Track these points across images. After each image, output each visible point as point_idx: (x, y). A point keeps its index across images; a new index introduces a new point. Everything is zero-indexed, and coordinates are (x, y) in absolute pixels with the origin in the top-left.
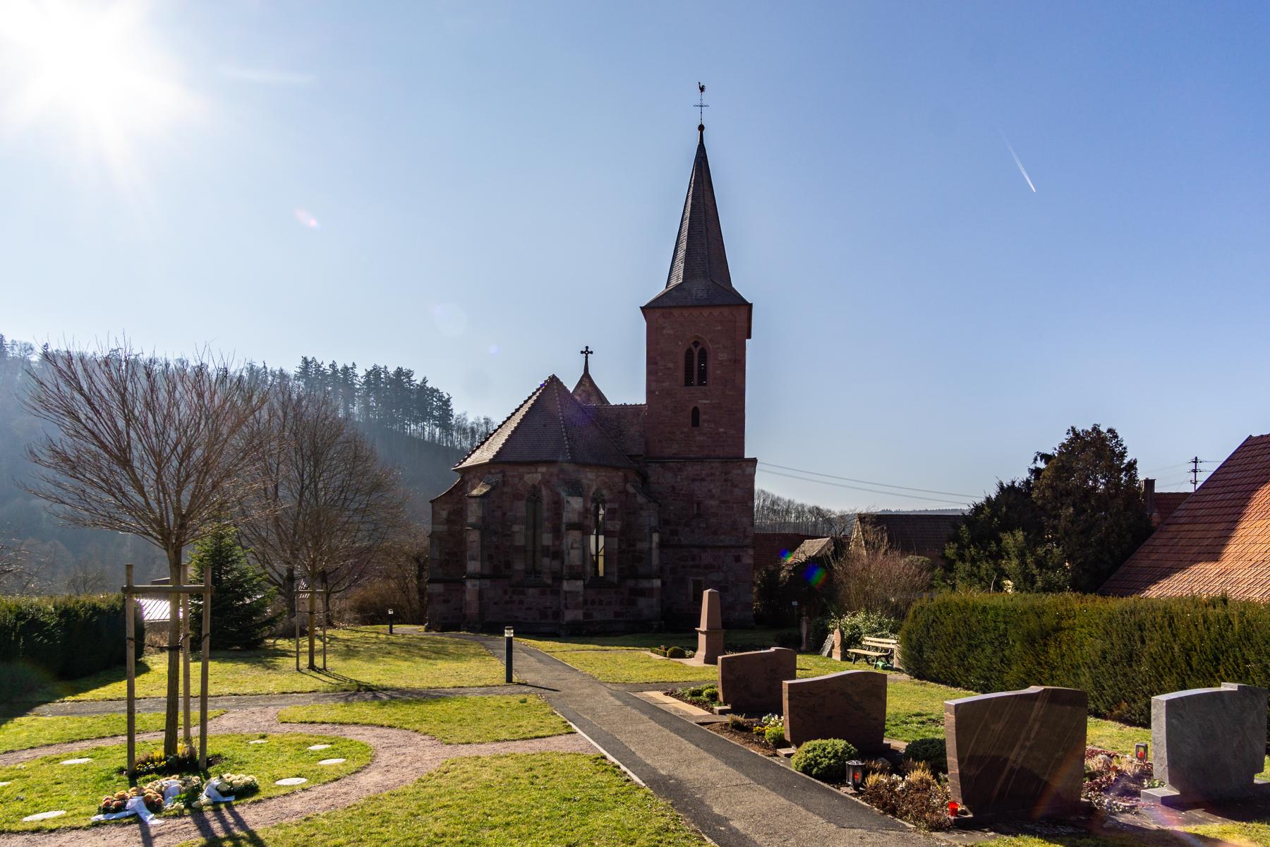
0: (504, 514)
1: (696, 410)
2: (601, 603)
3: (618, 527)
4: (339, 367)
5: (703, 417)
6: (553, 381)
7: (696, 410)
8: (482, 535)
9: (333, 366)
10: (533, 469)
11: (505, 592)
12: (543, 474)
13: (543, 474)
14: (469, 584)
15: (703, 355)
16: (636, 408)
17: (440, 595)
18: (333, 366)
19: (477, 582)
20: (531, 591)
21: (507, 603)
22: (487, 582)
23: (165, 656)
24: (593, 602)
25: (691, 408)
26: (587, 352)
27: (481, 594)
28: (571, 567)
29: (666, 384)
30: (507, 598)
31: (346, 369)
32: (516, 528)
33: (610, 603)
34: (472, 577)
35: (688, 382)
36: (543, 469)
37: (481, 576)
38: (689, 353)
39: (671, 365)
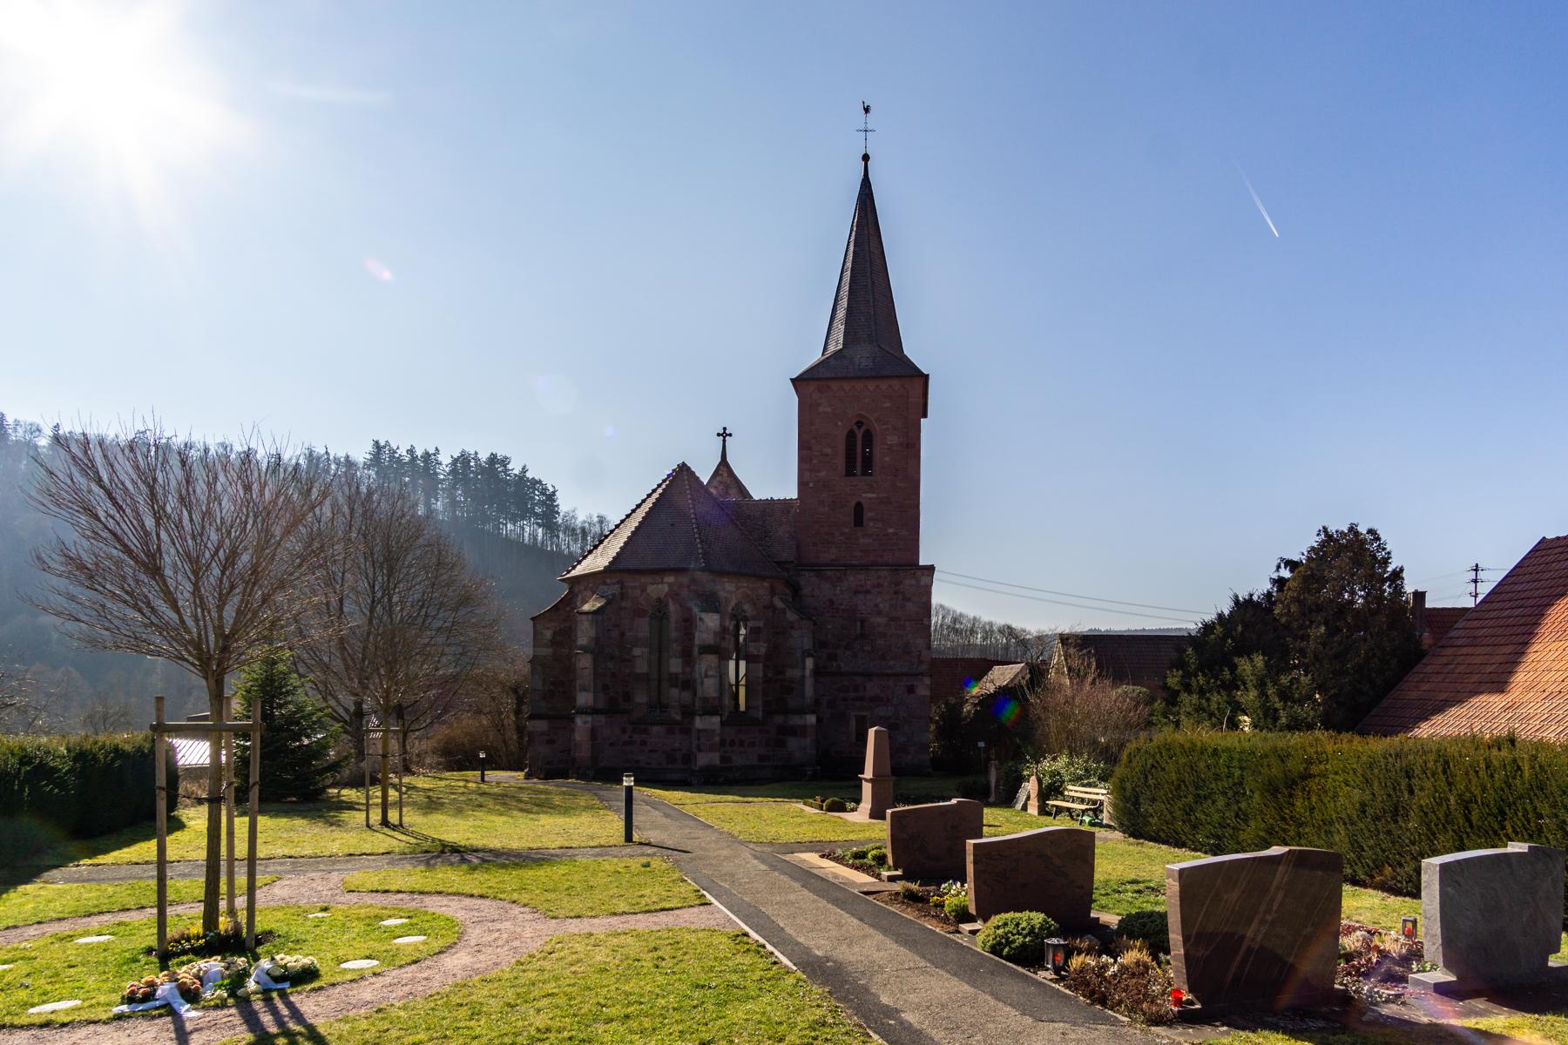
0: (623, 634)
1: (859, 506)
2: (742, 744)
3: (763, 650)
4: (419, 453)
5: (868, 515)
6: (683, 470)
7: (859, 506)
8: (595, 660)
9: (411, 451)
10: (658, 579)
11: (624, 731)
12: (670, 585)
13: (670, 585)
14: (579, 721)
15: (868, 438)
16: (786, 504)
17: (543, 734)
18: (411, 451)
19: (589, 718)
20: (655, 729)
21: (625, 743)
22: (602, 719)
24: (732, 743)
25: (853, 503)
26: (724, 434)
27: (593, 733)
28: (705, 700)
29: (823, 474)
30: (626, 737)
31: (427, 455)
32: (637, 651)
33: (753, 744)
34: (583, 711)
35: (849, 472)
36: (670, 579)
37: (594, 711)
38: (851, 436)
39: (828, 451)
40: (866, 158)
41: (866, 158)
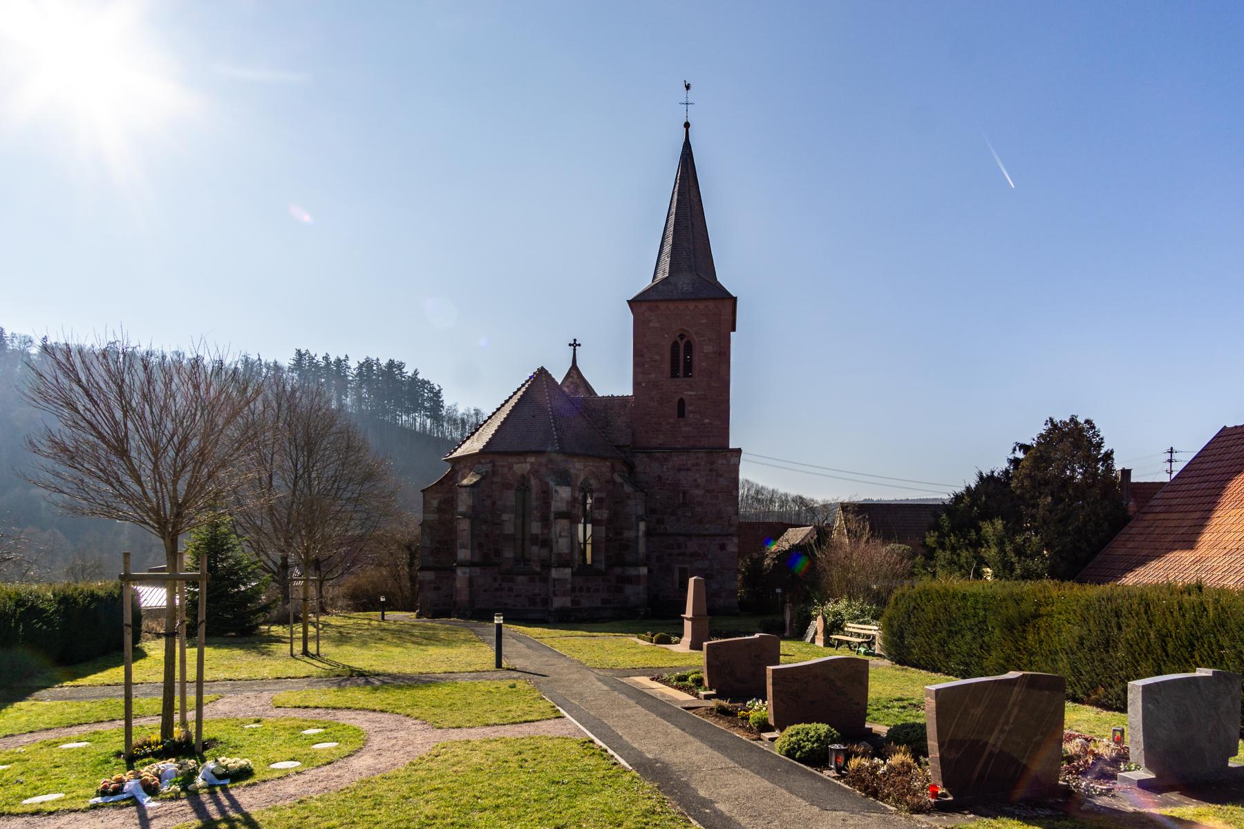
0: (494, 503)
1: (681, 402)
2: (588, 590)
3: (605, 516)
4: (332, 359)
5: (688, 408)
6: (542, 373)
7: (681, 402)
8: (472, 524)
9: (326, 358)
10: (522, 459)
11: (495, 580)
12: (532, 464)
13: (532, 464)
14: (459, 572)
15: (689, 347)
16: (623, 400)
17: (431, 582)
18: (326, 358)
19: (467, 570)
20: (520, 578)
21: (496, 590)
22: (477, 570)
23: (162, 642)
24: (581, 590)
25: (677, 399)
26: (575, 345)
27: (471, 581)
28: (559, 555)
29: (653, 376)
30: (496, 585)
31: (339, 361)
32: (505, 517)
33: (597, 590)
34: (462, 564)
35: (674, 374)
36: (532, 459)
37: (471, 564)
38: (675, 346)
39: (657, 357)
40: (687, 125)
41: (687, 125)
